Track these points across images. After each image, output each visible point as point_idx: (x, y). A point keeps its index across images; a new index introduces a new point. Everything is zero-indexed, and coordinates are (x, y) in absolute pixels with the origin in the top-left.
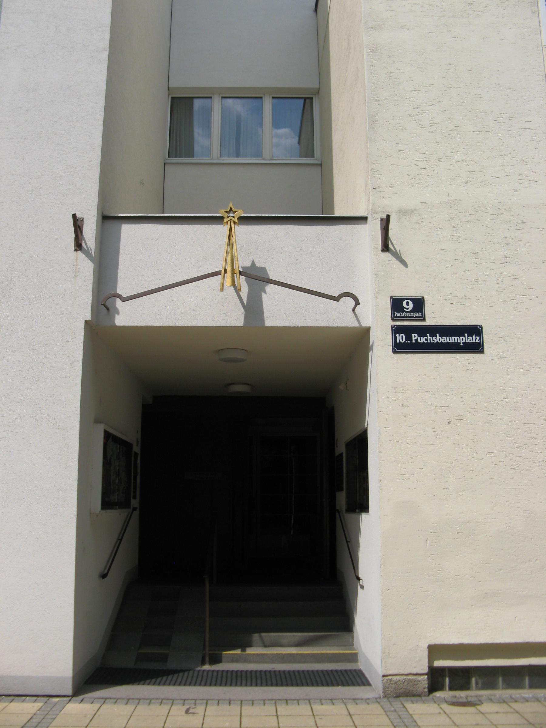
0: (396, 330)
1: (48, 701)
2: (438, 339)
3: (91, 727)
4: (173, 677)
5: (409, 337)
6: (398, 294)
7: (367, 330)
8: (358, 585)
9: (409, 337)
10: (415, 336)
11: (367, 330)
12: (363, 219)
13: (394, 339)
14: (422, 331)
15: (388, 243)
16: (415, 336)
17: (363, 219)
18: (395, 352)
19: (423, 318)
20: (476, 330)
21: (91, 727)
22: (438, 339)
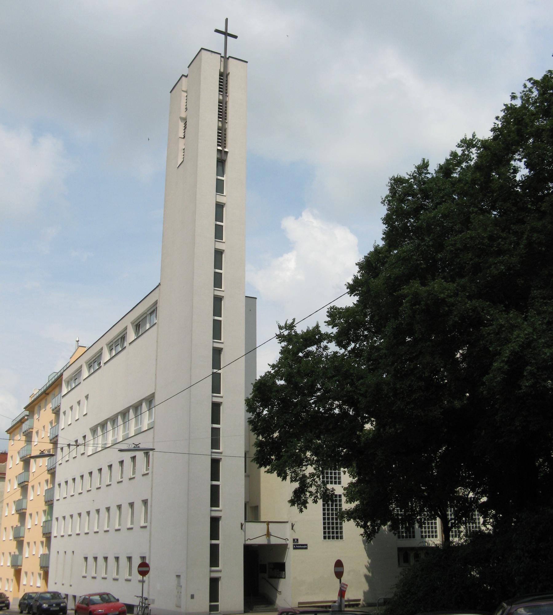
0: (294, 545)
1: (186, 104)
2: (300, 547)
3: (105, 363)
4: (20, 481)
5: (296, 546)
6: (294, 538)
7: (288, 544)
8: (499, 611)
9: (296, 546)
10: (297, 546)
11: (288, 544)
12: (287, 522)
13: (293, 547)
14: (298, 545)
15: (257, 546)
16: (297, 546)
17: (287, 522)
18: (293, 549)
19: (298, 543)
20: (306, 545)
21: (105, 363)
22: (300, 547)
